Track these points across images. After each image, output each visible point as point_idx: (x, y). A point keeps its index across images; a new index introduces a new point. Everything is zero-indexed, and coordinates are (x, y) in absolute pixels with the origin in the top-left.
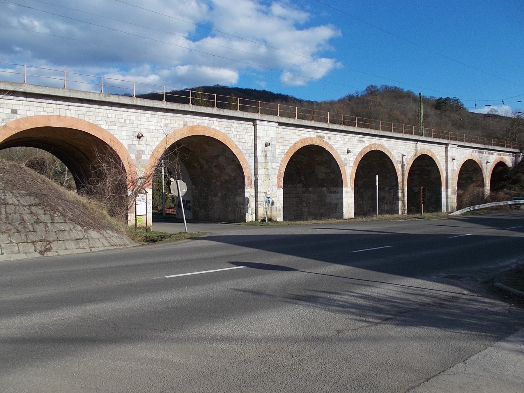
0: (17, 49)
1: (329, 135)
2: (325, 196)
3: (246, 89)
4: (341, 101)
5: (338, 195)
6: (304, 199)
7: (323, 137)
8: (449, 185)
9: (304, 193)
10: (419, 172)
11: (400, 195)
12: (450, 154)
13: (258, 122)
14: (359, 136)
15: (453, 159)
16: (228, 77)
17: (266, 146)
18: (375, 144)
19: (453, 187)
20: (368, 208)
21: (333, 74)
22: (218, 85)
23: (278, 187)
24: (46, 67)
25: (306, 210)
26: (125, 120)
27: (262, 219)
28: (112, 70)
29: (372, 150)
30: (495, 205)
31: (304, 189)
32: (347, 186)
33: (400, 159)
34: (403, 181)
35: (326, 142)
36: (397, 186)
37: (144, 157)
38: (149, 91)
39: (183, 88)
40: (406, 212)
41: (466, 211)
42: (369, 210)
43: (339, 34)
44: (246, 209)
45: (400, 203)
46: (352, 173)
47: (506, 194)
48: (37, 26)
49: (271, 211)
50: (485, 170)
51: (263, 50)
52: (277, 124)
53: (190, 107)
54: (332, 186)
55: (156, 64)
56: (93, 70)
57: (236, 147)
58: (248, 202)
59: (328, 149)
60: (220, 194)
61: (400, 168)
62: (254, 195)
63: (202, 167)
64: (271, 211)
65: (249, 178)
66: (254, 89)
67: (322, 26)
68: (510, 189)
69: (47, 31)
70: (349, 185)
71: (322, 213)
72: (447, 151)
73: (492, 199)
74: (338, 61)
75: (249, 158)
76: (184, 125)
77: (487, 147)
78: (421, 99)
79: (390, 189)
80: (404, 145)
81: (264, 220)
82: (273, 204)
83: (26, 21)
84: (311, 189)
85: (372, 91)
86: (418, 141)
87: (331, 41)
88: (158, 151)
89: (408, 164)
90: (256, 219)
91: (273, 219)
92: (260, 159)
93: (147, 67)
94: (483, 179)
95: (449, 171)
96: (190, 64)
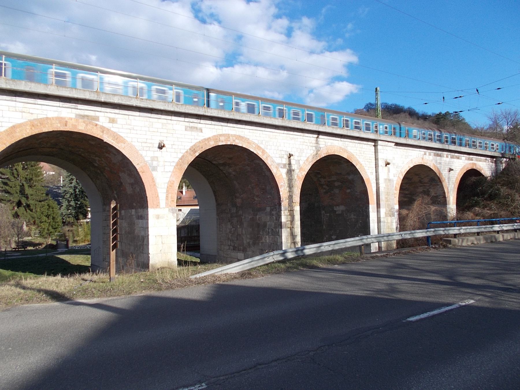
5: (144, 221)
7: (97, 119)
8: (382, 203)
10: (340, 184)
11: (284, 218)
12: (380, 156)
14: (187, 119)
15: (387, 164)
18: (228, 136)
19: (388, 205)
20: (248, 241)
29: (220, 144)
32: (158, 206)
33: (285, 161)
34: (291, 197)
36: (280, 205)
45: (285, 234)
47: (477, 215)
50: (447, 181)
59: (107, 139)
61: (284, 176)
68: (485, 207)
70: (163, 202)
72: (376, 152)
73: (459, 222)
77: (446, 147)
79: (272, 210)
80: (293, 138)
86: (319, 133)
89: (301, 169)
94: (444, 193)
95: (381, 181)
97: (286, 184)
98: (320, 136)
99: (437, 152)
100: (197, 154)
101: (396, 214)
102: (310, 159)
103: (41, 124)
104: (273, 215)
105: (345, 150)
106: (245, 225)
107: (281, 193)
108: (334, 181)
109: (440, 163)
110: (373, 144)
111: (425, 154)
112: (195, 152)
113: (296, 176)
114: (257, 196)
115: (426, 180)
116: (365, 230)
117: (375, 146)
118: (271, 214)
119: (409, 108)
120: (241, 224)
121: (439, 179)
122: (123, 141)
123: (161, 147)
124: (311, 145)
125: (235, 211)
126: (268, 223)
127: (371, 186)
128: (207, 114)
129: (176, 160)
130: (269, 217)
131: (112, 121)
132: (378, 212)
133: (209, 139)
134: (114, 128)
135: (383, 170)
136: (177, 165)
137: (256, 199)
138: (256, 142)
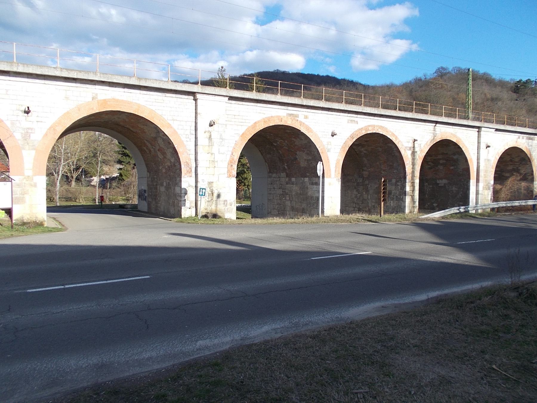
0: (95, 37)
1: (306, 114)
2: (307, 188)
3: (308, 74)
4: (406, 86)
6: (287, 191)
7: (297, 116)
8: (481, 179)
9: (287, 184)
11: (408, 188)
12: (482, 140)
13: (198, 96)
14: (349, 115)
16: (294, 63)
17: (211, 125)
18: (374, 126)
19: (486, 180)
20: (373, 204)
21: (407, 57)
22: (278, 70)
23: (230, 176)
24: (119, 55)
25: (288, 203)
26: (7, 90)
27: (204, 214)
28: (181, 56)
29: (369, 132)
30: (504, 205)
31: (287, 179)
32: (330, 177)
33: (411, 145)
34: (413, 172)
35: (301, 122)
36: (405, 178)
37: (33, 137)
38: (207, 77)
39: (249, 72)
40: (416, 210)
41: (452, 212)
42: (374, 206)
43: (416, 12)
44: (183, 202)
45: (408, 199)
46: (338, 161)
48: (115, 15)
49: (216, 204)
51: (333, 32)
52: (227, 98)
53: (253, 95)
54: (314, 177)
55: (224, 50)
56: (164, 57)
57: (170, 126)
58: (186, 194)
59: (303, 130)
60: (165, 184)
62: (194, 185)
63: (150, 151)
64: (216, 204)
65: (187, 164)
66: (316, 74)
67: (397, 5)
69: (123, 20)
71: (303, 209)
72: (479, 137)
74: (414, 42)
75: (188, 140)
76: (93, 98)
78: (471, 76)
79: (397, 182)
81: (205, 216)
82: (219, 196)
83: (103, 10)
84: (293, 179)
85: (442, 73)
86: (437, 122)
87: (407, 21)
88: (54, 130)
89: (421, 151)
90: (196, 214)
91: (219, 214)
92: (202, 139)
93: (216, 53)
94: (533, 171)
96: (259, 49)
97: (411, 163)
98: (437, 125)
99: (529, 136)
100: (354, 140)
101: (491, 188)
102: (429, 143)
103: (269, 121)
104: (398, 185)
105: (455, 136)
106: (371, 192)
107: (406, 170)
108: (441, 159)
109: (531, 146)
110: (477, 130)
111: (519, 138)
112: (353, 138)
113: (418, 156)
114: (384, 170)
115: (517, 160)
116: (465, 201)
117: (478, 131)
118: (396, 185)
119: (484, 74)
120: (367, 191)
121: (529, 159)
122: (311, 131)
123: (333, 135)
124: (430, 132)
125: (361, 181)
126: (393, 192)
127: (473, 164)
128: (364, 111)
129: (342, 144)
130: (394, 187)
131: (306, 117)
132: (477, 186)
133: (361, 129)
134: (306, 122)
135: (483, 151)
136: (342, 148)
137: (383, 172)
138: (392, 131)
